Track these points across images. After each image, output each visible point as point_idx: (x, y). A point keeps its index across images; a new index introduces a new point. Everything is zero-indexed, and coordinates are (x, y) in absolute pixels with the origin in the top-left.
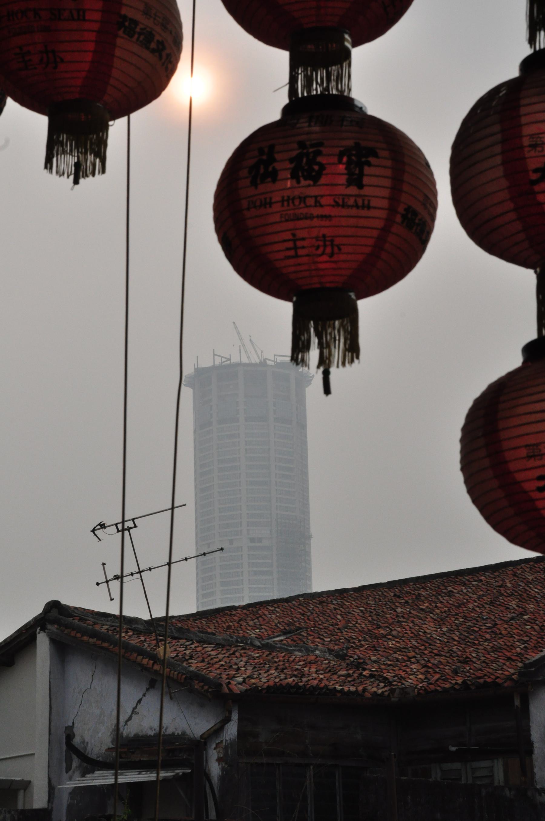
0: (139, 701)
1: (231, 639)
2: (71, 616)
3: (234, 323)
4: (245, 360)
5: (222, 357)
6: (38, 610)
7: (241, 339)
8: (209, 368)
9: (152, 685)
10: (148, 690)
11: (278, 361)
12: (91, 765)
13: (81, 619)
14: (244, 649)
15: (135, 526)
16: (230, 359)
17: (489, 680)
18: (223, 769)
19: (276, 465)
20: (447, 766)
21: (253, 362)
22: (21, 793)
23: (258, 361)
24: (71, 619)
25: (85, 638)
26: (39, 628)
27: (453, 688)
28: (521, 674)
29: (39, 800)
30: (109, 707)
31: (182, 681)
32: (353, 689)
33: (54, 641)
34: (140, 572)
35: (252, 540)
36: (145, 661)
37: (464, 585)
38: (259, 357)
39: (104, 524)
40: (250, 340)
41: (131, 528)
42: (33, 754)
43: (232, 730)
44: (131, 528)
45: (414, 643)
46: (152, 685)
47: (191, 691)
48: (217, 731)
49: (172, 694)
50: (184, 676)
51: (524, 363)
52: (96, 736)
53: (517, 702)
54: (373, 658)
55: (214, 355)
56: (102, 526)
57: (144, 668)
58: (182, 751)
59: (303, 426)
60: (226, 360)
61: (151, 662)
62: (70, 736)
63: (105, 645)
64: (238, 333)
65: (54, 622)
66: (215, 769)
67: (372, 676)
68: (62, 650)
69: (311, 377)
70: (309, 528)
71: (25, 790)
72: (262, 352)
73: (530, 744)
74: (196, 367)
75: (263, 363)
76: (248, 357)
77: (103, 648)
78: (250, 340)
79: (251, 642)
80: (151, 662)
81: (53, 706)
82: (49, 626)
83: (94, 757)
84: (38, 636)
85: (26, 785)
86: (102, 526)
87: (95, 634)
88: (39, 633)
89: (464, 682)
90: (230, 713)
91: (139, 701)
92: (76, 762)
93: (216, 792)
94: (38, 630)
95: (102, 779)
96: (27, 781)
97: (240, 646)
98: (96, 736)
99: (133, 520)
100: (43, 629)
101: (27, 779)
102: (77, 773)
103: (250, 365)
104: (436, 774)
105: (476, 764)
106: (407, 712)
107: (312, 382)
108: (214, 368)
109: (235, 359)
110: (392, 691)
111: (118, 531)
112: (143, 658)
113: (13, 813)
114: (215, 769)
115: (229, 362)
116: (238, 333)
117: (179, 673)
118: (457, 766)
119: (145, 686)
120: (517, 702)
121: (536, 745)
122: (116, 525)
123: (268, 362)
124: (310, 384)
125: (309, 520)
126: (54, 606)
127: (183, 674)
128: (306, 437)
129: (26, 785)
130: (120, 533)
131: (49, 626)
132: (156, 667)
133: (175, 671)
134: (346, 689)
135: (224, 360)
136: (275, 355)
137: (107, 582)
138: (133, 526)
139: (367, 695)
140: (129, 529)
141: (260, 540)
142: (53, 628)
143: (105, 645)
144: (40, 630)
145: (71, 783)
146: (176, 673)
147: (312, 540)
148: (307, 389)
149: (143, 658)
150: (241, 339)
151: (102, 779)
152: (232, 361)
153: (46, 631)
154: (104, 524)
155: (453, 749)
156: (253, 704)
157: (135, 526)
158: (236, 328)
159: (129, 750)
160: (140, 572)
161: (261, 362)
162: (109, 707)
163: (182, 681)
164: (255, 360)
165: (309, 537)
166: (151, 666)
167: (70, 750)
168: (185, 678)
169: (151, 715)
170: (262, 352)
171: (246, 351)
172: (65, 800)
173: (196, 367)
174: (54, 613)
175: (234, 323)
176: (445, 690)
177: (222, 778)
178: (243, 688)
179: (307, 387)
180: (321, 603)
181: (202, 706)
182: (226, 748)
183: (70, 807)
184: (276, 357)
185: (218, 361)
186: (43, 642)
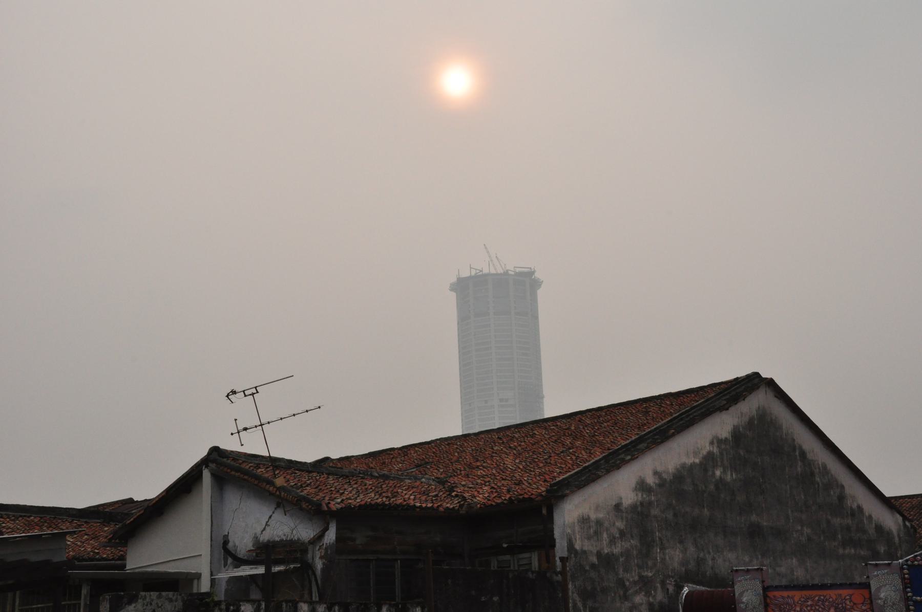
0: (270, 517)
2: (228, 458)
4: (493, 271)
6: (204, 453)
9: (278, 506)
12: (239, 562)
13: (234, 459)
14: (363, 478)
17: (526, 496)
18: (324, 564)
20: (501, 558)
22: (195, 582)
24: (225, 460)
25: (233, 473)
27: (502, 503)
28: (547, 491)
29: (205, 587)
30: (255, 521)
32: (430, 505)
33: (214, 475)
34: (261, 425)
35: (501, 400)
37: (546, 428)
43: (331, 536)
45: (494, 471)
46: (278, 506)
47: (301, 509)
48: (321, 536)
52: (243, 543)
53: (544, 511)
54: (463, 483)
56: (234, 392)
57: (271, 494)
58: (289, 550)
59: (536, 317)
62: (226, 542)
63: (246, 477)
65: (214, 461)
66: (319, 565)
67: (456, 496)
68: (220, 481)
73: (554, 540)
75: (506, 273)
77: (245, 480)
82: (210, 465)
83: (241, 556)
85: (198, 576)
86: (234, 392)
87: (238, 470)
89: (510, 498)
90: (328, 524)
91: (270, 517)
92: (230, 560)
93: (319, 582)
95: (246, 571)
98: (243, 543)
100: (207, 467)
102: (231, 567)
103: (497, 274)
104: (494, 565)
105: (521, 556)
106: (476, 520)
109: (486, 271)
110: (461, 506)
114: (319, 565)
118: (508, 557)
119: (274, 506)
120: (544, 511)
121: (557, 541)
123: (510, 272)
126: (215, 450)
129: (198, 576)
131: (210, 465)
134: (424, 505)
137: (238, 432)
139: (441, 509)
140: (253, 394)
142: (213, 466)
143: (246, 477)
145: (224, 575)
147: (545, 399)
151: (246, 571)
155: (505, 546)
156: (347, 517)
159: (266, 551)
160: (261, 425)
162: (255, 521)
164: (500, 271)
165: (543, 397)
167: (225, 552)
169: (284, 527)
172: (223, 586)
174: (215, 455)
176: (498, 504)
177: (323, 570)
178: (339, 506)
180: (448, 444)
181: (311, 520)
182: (326, 549)
183: (226, 590)
185: (473, 273)
186: (206, 475)
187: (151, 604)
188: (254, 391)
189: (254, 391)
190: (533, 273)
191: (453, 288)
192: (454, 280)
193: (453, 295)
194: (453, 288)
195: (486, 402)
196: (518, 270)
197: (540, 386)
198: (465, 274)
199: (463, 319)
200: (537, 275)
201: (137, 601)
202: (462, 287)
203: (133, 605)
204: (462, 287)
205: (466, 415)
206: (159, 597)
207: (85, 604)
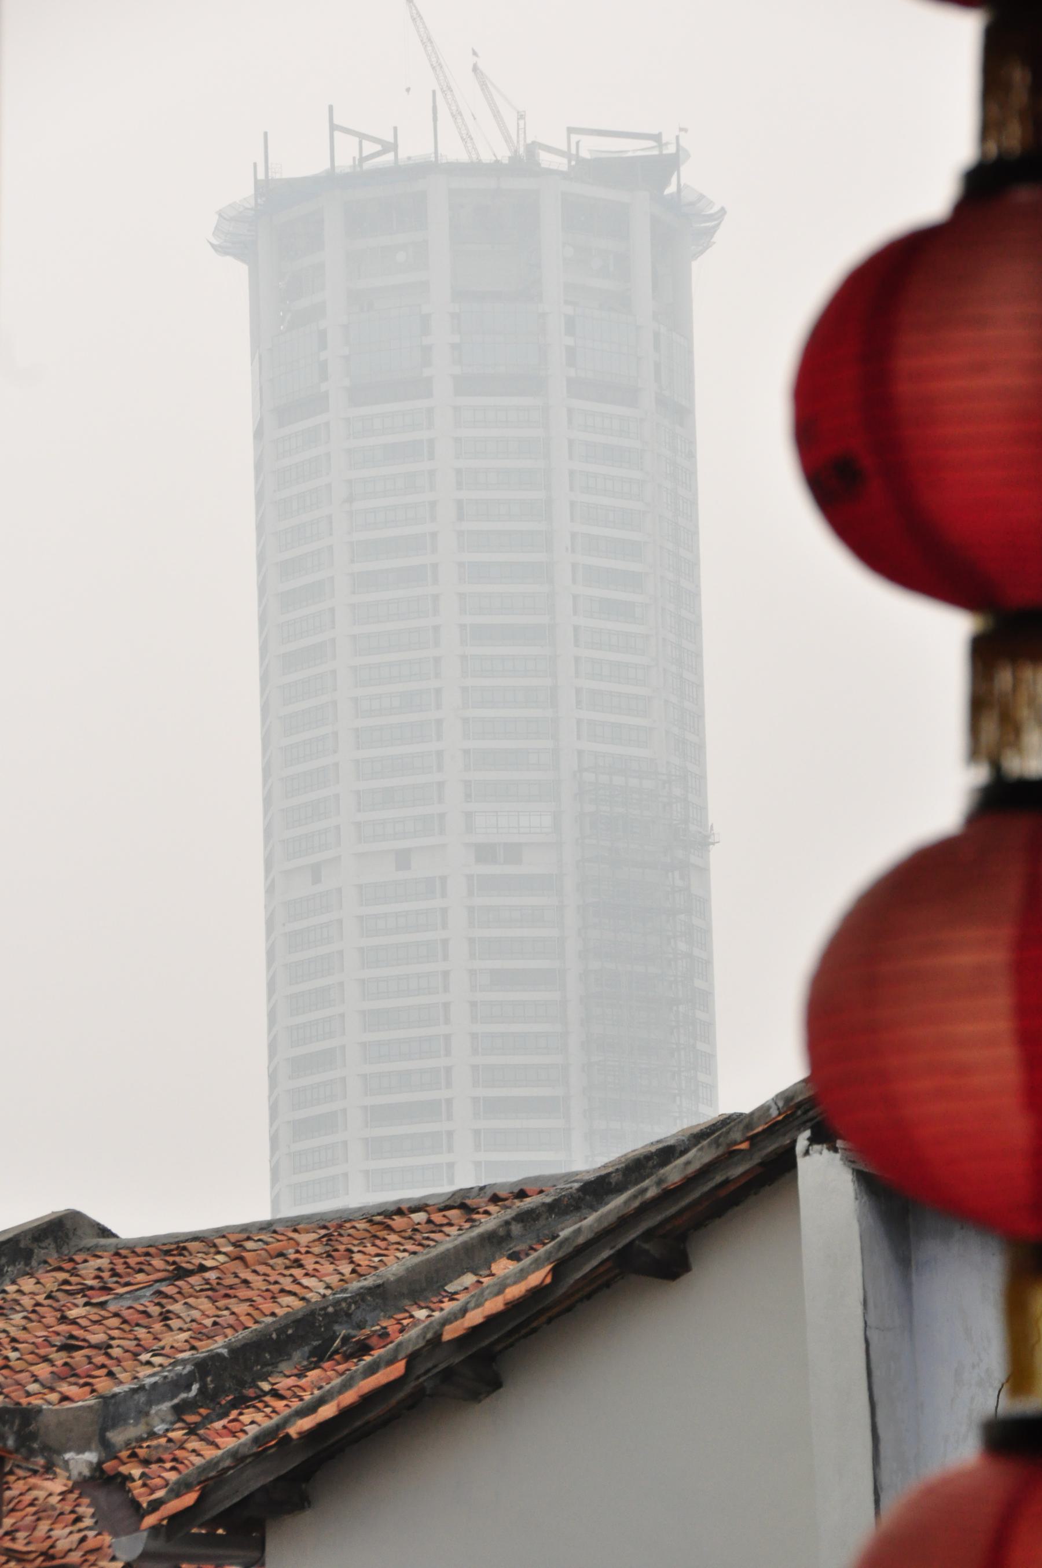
4: (453, 151)
12: (139, 1256)
35: (484, 853)
75: (524, 163)
103: (473, 169)
109: (414, 147)
123: (547, 160)
147: (716, 855)
164: (493, 148)
165: (704, 842)
186: (825, 1179)
191: (238, 236)
192: (241, 191)
193: (235, 274)
194: (238, 236)
195: (403, 859)
196: (589, 147)
198: (302, 159)
199: (286, 410)
200: (692, 177)
202: (280, 228)
204: (280, 228)
205: (298, 1127)
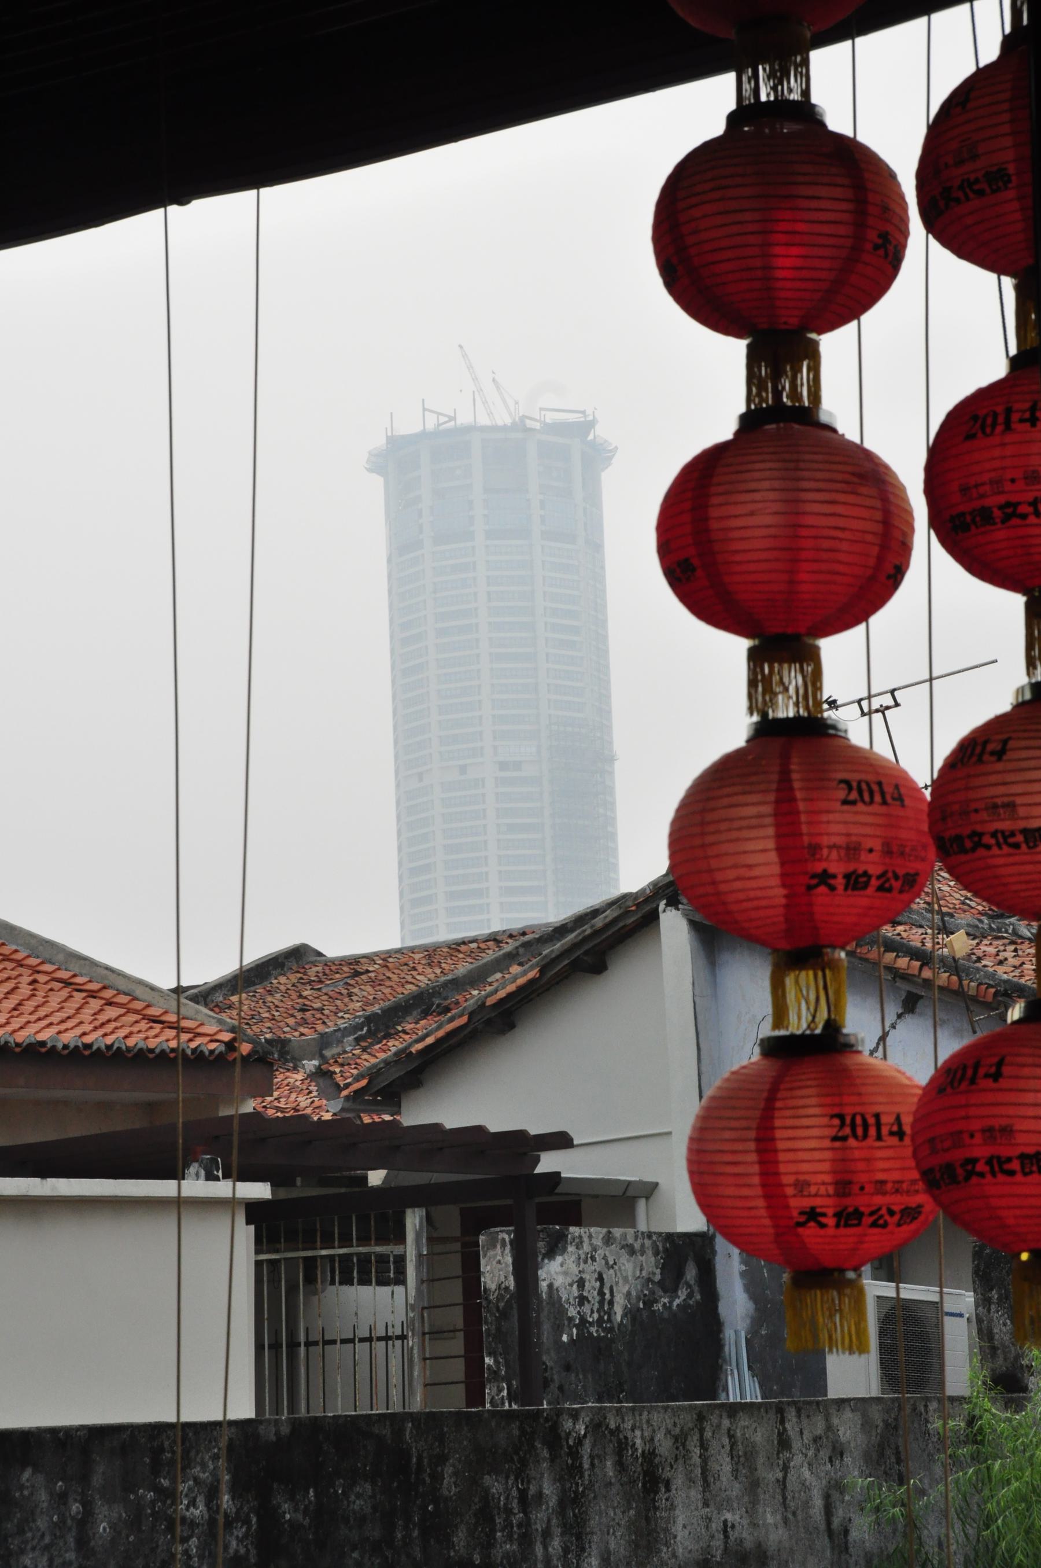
1: (980, 925)
3: (461, 347)
4: (484, 420)
5: (439, 414)
7: (475, 379)
8: (416, 435)
9: (910, 1005)
10: (899, 1016)
11: (548, 421)
15: (897, 705)
16: (454, 419)
19: (546, 623)
21: (500, 423)
22: (641, 1204)
23: (508, 421)
26: (665, 902)
31: (989, 998)
35: (503, 766)
36: (903, 962)
38: (510, 414)
39: (835, 701)
40: (494, 380)
41: (888, 708)
42: (670, 1133)
44: (888, 708)
49: (976, 1025)
50: (993, 990)
51: (737, 434)
55: (424, 410)
57: (898, 975)
60: (446, 419)
61: (918, 964)
64: (470, 367)
69: (610, 451)
70: (611, 743)
71: (647, 1198)
72: (517, 403)
74: (389, 434)
76: (490, 414)
78: (494, 380)
79: (1014, 929)
80: (918, 964)
81: (702, 1046)
84: (662, 916)
88: (664, 911)
94: (662, 905)
96: (652, 1183)
97: (1003, 938)
99: (892, 692)
101: (654, 1180)
103: (494, 428)
107: (614, 461)
108: (424, 435)
109: (464, 418)
111: (863, 714)
112: (897, 956)
113: (654, 1238)
115: (452, 423)
116: (470, 367)
117: (980, 984)
119: (892, 1010)
122: (859, 702)
123: (529, 423)
124: (610, 464)
125: (610, 727)
127: (990, 986)
128: (603, 568)
129: (649, 1190)
130: (867, 718)
132: (927, 974)
133: (971, 980)
135: (442, 419)
136: (541, 409)
138: (892, 703)
140: (883, 710)
141: (517, 765)
144: (667, 905)
146: (972, 984)
147: (617, 764)
148: (604, 475)
149: (897, 956)
150: (475, 379)
152: (459, 422)
153: (680, 906)
154: (835, 701)
157: (897, 705)
158: (465, 356)
161: (514, 423)
163: (989, 998)
164: (503, 419)
165: (612, 759)
166: (916, 972)
168: (996, 994)
170: (517, 403)
171: (485, 402)
173: (389, 434)
175: (461, 347)
179: (603, 470)
184: (543, 413)
185: (431, 424)
187: (593, 1259)
188: (888, 700)
189: (888, 700)
190: (590, 425)
191: (378, 463)
192: (380, 441)
193: (377, 482)
194: (378, 463)
195: (463, 769)
196: (550, 417)
197: (606, 728)
198: (409, 425)
199: (403, 547)
201: (564, 1250)
203: (559, 1259)
206: (608, 1240)
207: (420, 1256)
